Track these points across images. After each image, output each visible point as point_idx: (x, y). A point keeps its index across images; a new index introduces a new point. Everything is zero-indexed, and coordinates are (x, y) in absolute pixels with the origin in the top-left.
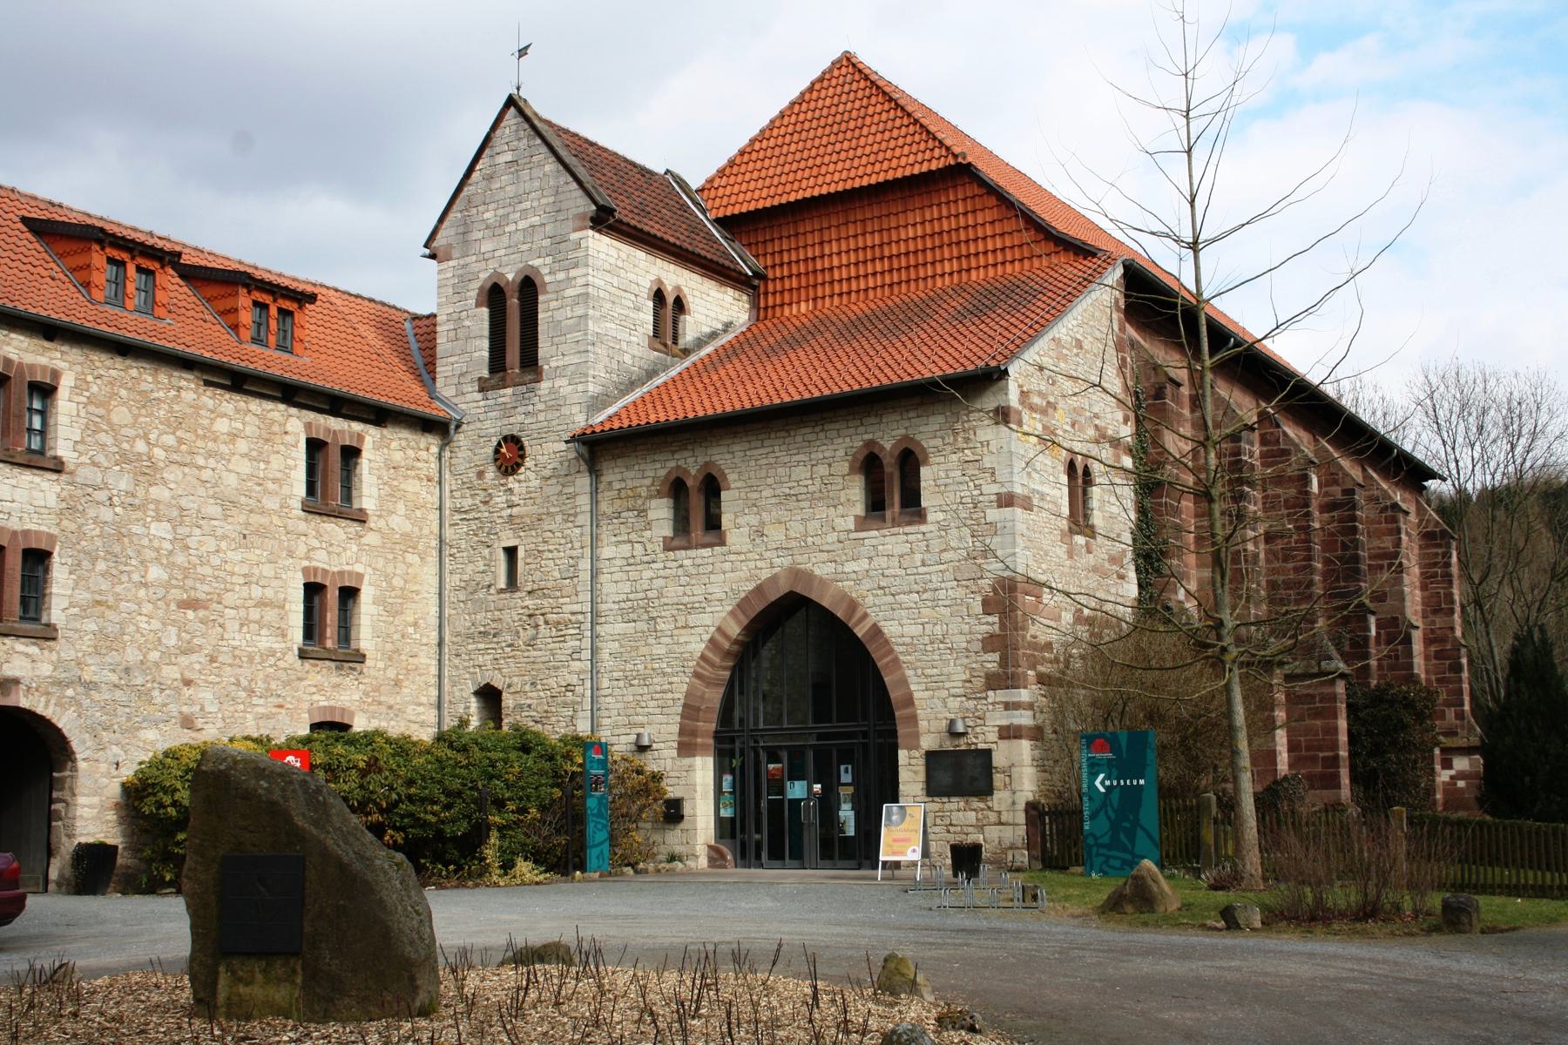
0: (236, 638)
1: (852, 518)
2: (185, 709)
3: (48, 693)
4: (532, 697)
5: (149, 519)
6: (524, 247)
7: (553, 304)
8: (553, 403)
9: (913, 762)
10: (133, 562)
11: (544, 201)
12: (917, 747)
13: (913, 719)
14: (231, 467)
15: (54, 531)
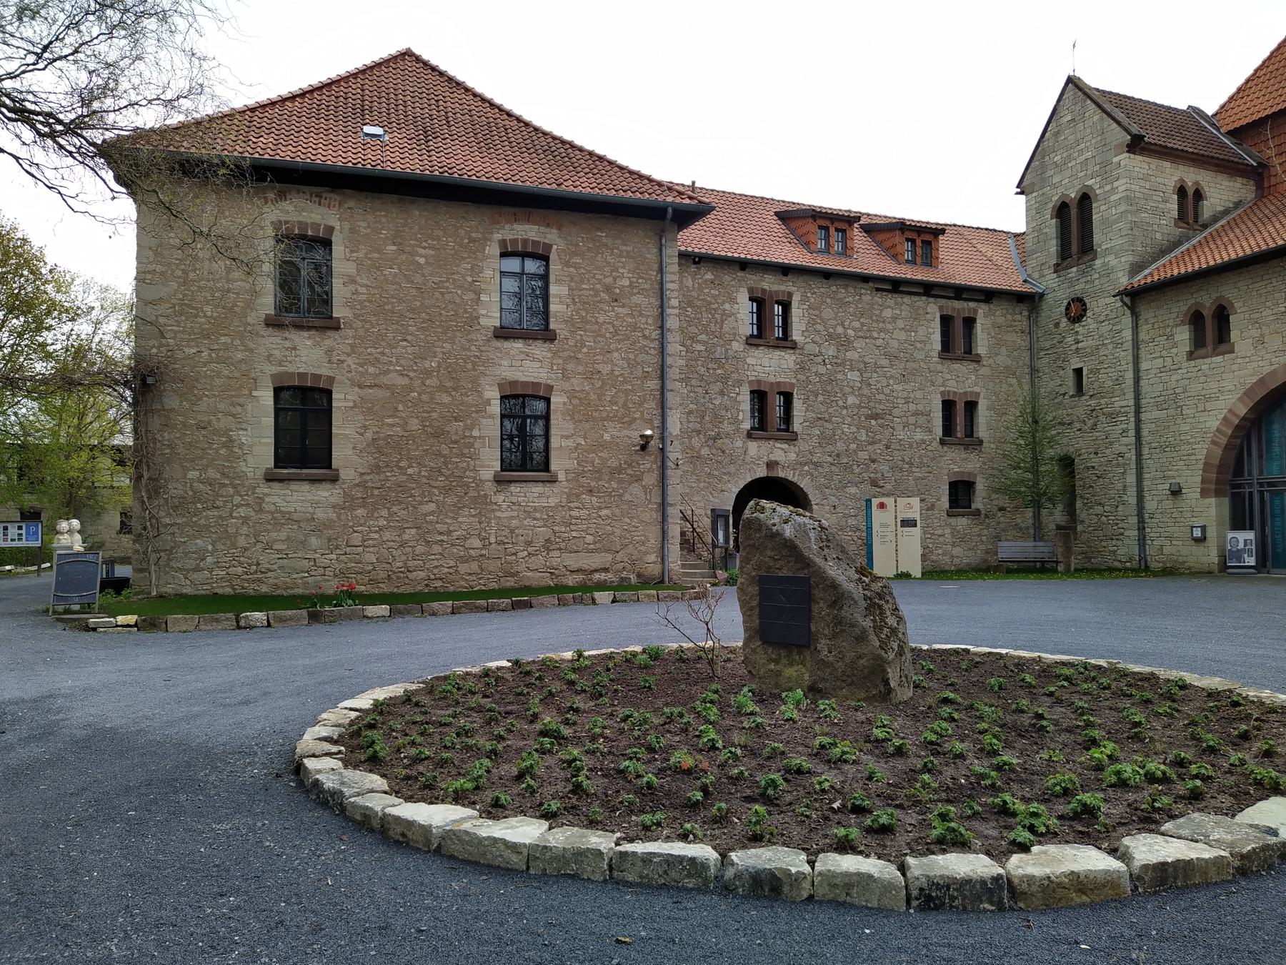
0: (901, 435)
2: (872, 475)
4: (1095, 461)
6: (1083, 174)
7: (1103, 208)
10: (838, 395)
11: (1094, 141)
14: (894, 337)
15: (794, 381)
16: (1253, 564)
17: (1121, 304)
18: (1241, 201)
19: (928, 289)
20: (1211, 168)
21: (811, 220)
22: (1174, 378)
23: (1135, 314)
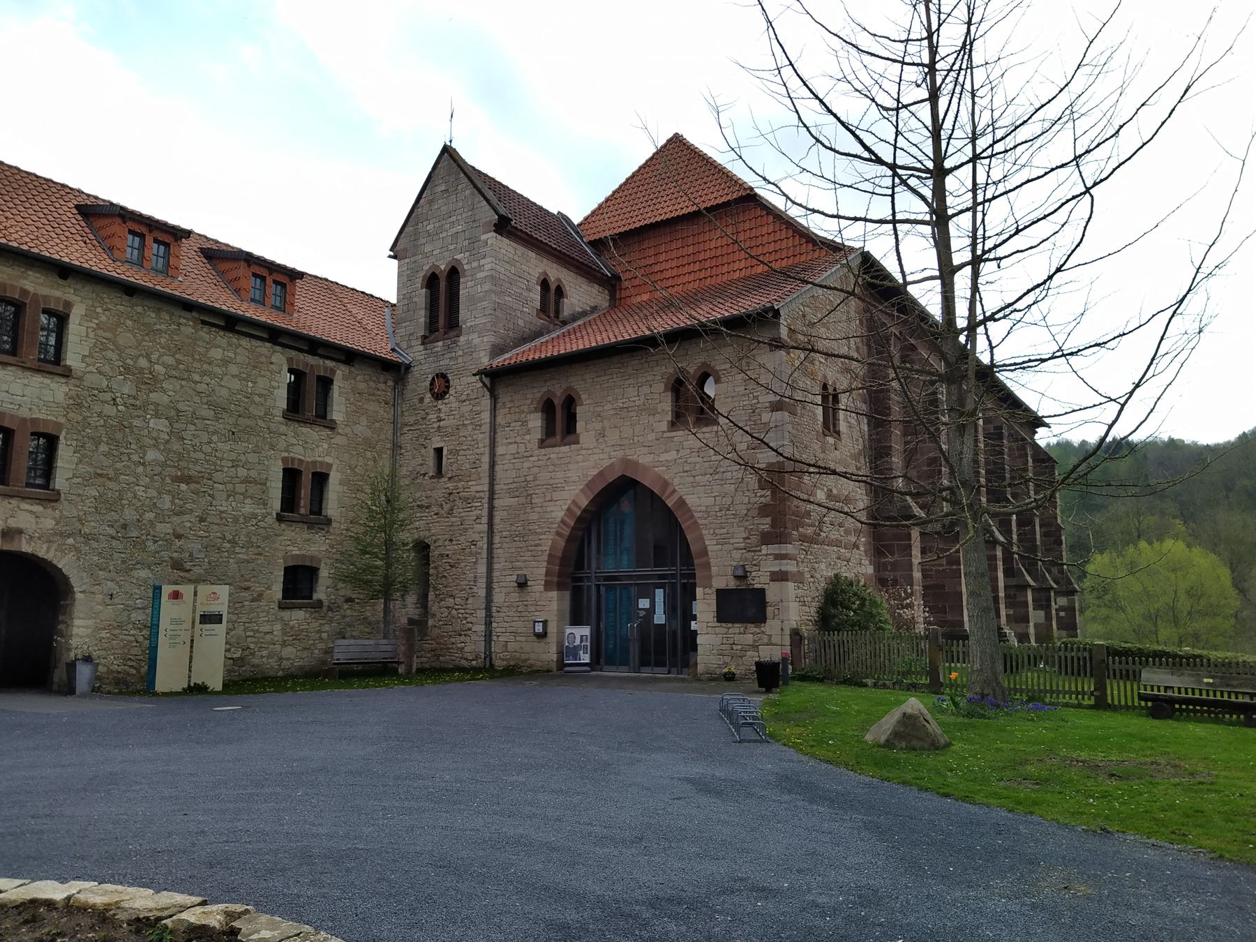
1: (666, 423)
2: (175, 555)
3: (49, 541)
4: (450, 549)
5: (148, 416)
7: (469, 284)
8: (468, 350)
9: (707, 596)
11: (464, 215)
12: (711, 587)
13: (707, 566)
15: (62, 420)
16: (587, 660)
17: (481, 385)
18: (596, 307)
19: (274, 335)
20: (572, 269)
21: (119, 220)
22: (526, 465)
23: (494, 397)
